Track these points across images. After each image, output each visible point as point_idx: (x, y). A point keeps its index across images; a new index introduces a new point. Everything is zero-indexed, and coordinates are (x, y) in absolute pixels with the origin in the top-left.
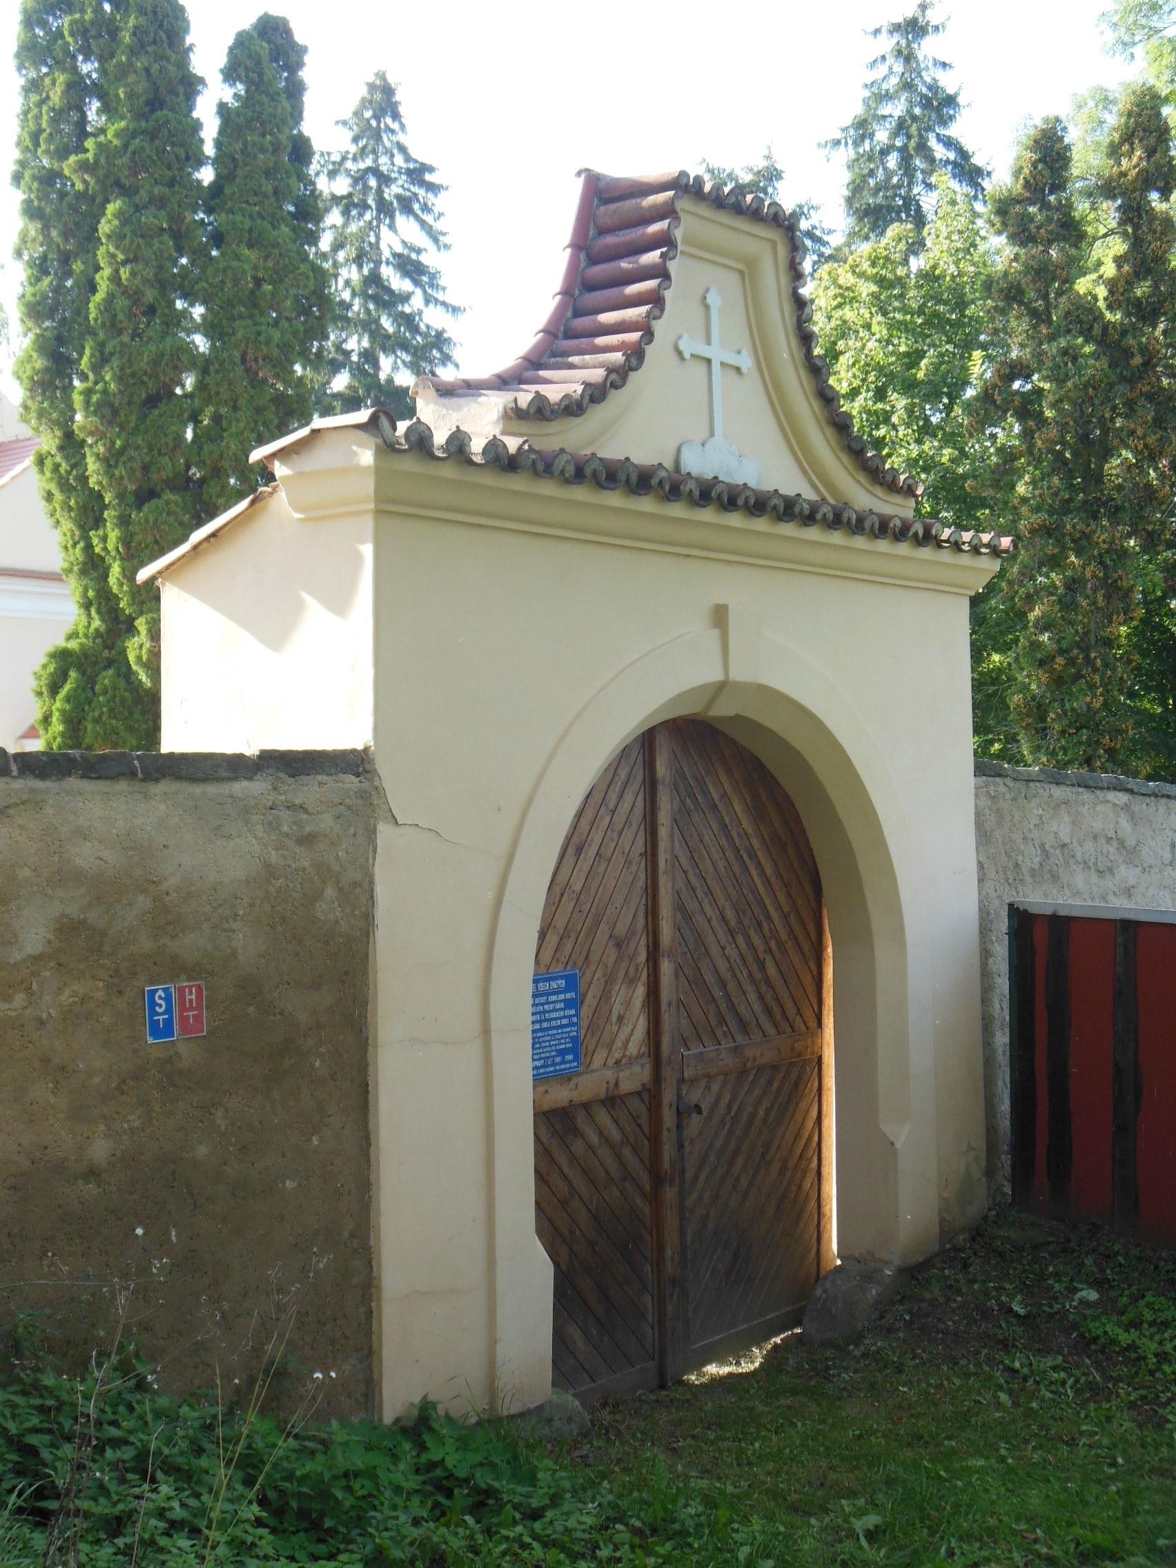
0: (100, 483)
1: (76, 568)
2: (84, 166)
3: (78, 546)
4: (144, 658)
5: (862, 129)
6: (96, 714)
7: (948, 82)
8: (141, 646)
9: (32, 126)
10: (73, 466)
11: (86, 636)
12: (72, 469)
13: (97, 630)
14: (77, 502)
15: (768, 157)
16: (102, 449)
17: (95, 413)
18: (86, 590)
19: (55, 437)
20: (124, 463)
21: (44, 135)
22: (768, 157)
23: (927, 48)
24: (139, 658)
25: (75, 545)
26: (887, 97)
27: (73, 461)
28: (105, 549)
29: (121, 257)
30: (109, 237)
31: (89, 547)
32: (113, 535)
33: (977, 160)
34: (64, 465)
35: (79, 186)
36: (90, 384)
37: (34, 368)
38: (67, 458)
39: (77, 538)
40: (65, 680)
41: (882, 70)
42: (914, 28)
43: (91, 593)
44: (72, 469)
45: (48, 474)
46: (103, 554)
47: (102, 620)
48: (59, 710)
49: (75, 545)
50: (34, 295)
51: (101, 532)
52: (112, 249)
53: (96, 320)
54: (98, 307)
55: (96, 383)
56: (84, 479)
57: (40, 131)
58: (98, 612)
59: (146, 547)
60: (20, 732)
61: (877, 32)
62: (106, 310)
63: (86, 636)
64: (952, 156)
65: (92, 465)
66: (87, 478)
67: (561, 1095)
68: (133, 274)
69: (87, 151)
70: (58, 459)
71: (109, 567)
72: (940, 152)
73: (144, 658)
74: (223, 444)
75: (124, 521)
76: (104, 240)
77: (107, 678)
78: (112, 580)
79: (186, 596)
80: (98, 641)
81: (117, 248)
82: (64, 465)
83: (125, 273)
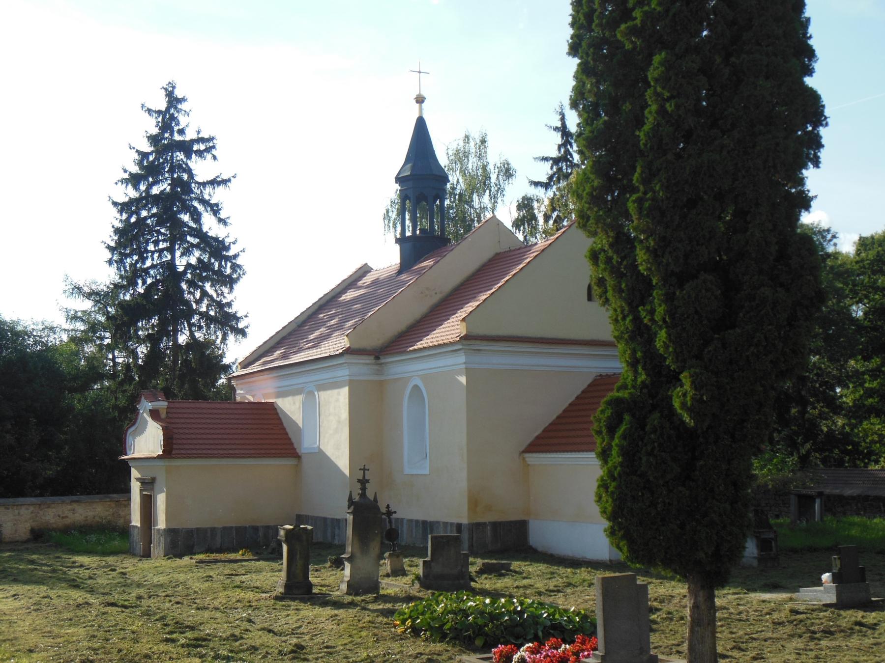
0: (649, 269)
1: (626, 336)
2: (633, 31)
3: (628, 320)
4: (689, 403)
6: (649, 448)
8: (685, 395)
9: (586, 9)
10: (623, 259)
11: (634, 387)
12: (622, 260)
13: (643, 382)
14: (627, 285)
16: (652, 243)
17: (648, 216)
18: (634, 352)
19: (608, 237)
20: (670, 252)
21: (597, 13)
24: (683, 405)
25: (624, 318)
27: (623, 254)
28: (652, 320)
29: (666, 94)
30: (656, 80)
31: (637, 320)
32: (660, 310)
34: (615, 257)
35: (628, 46)
36: (640, 194)
37: (592, 186)
38: (617, 252)
39: (626, 313)
40: (620, 421)
43: (639, 354)
44: (622, 260)
45: (602, 266)
46: (649, 324)
47: (647, 375)
48: (617, 445)
49: (624, 318)
50: (592, 132)
51: (648, 307)
52: (659, 89)
53: (645, 145)
54: (647, 134)
55: (645, 193)
56: (634, 267)
57: (593, 11)
58: (644, 369)
59: (688, 317)
60: (522, 449)
62: (654, 136)
63: (634, 387)
65: (641, 256)
66: (637, 266)
67: (405, 521)
68: (678, 107)
69: (636, 18)
70: (610, 253)
71: (656, 334)
73: (689, 403)
74: (749, 233)
75: (669, 298)
76: (652, 84)
77: (655, 419)
78: (658, 344)
80: (645, 391)
81: (663, 88)
82: (615, 257)
83: (669, 107)
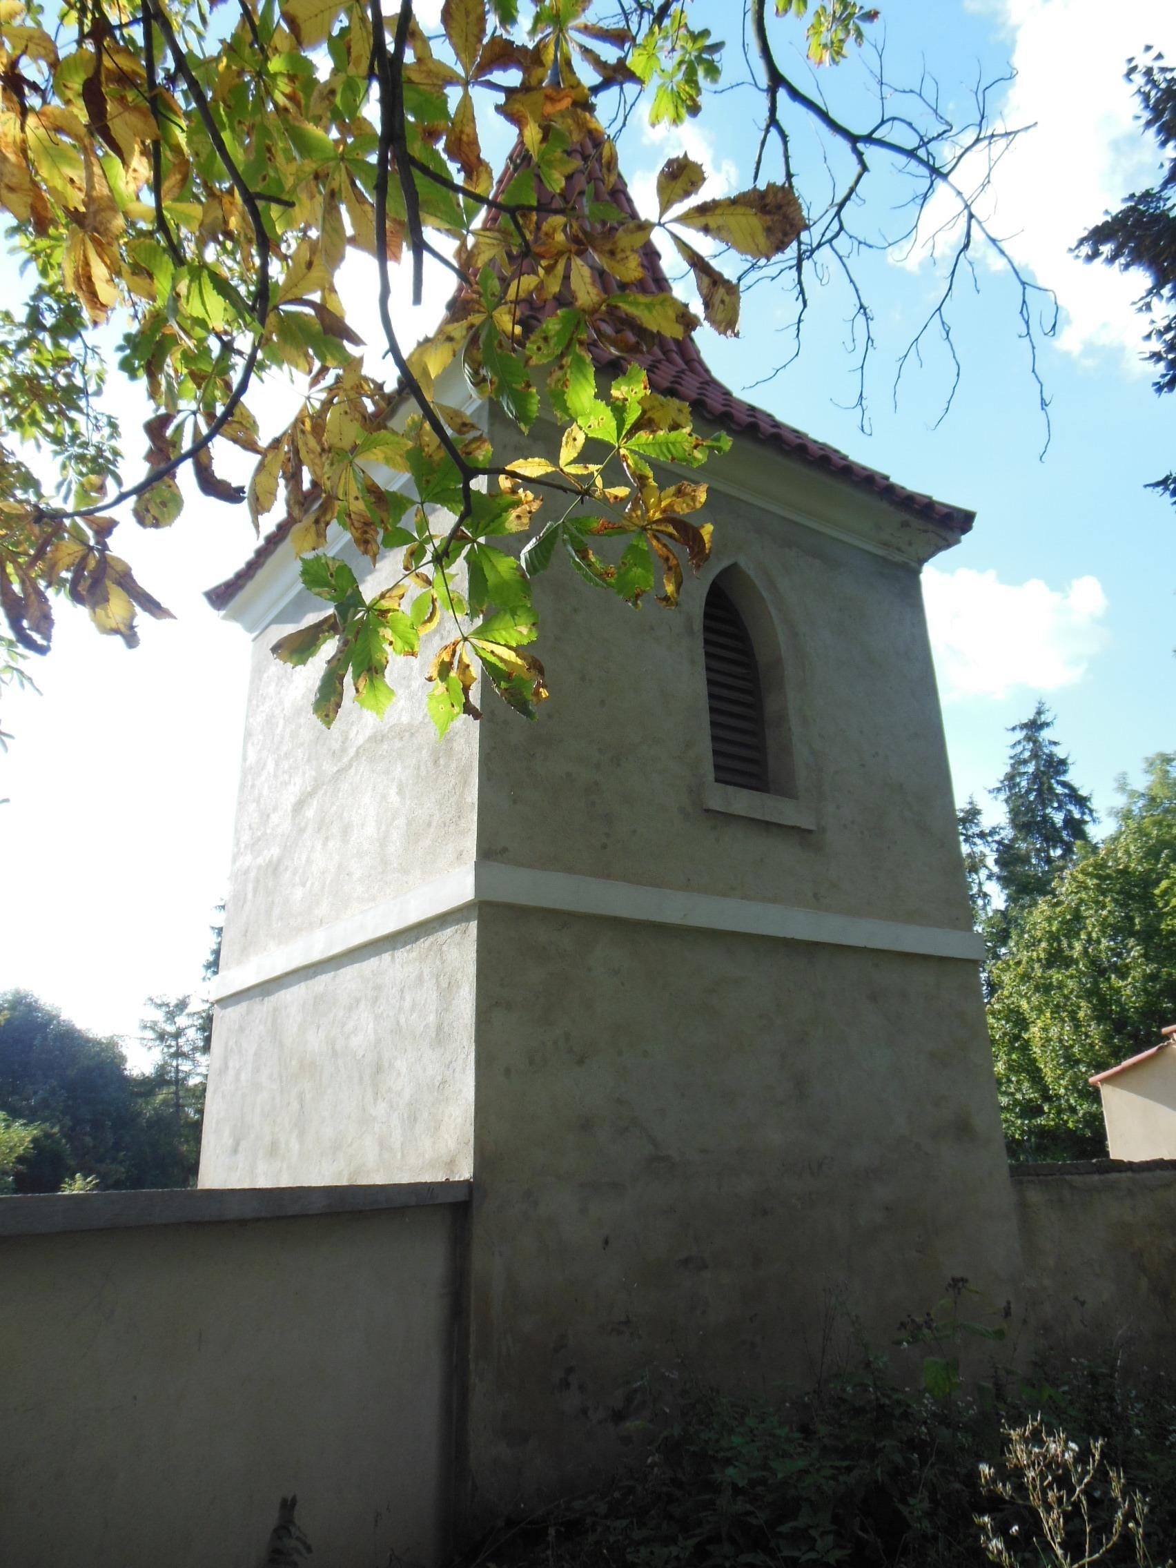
5: (1011, 778)
7: (1060, 752)
15: (971, 803)
22: (971, 803)
23: (1045, 735)
26: (1025, 762)
33: (1083, 792)
41: (1019, 748)
42: (1034, 726)
61: (1014, 729)
64: (1066, 791)
72: (1059, 790)
79: (1118, 1090)
